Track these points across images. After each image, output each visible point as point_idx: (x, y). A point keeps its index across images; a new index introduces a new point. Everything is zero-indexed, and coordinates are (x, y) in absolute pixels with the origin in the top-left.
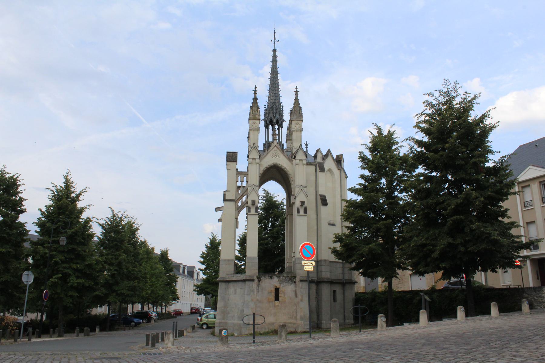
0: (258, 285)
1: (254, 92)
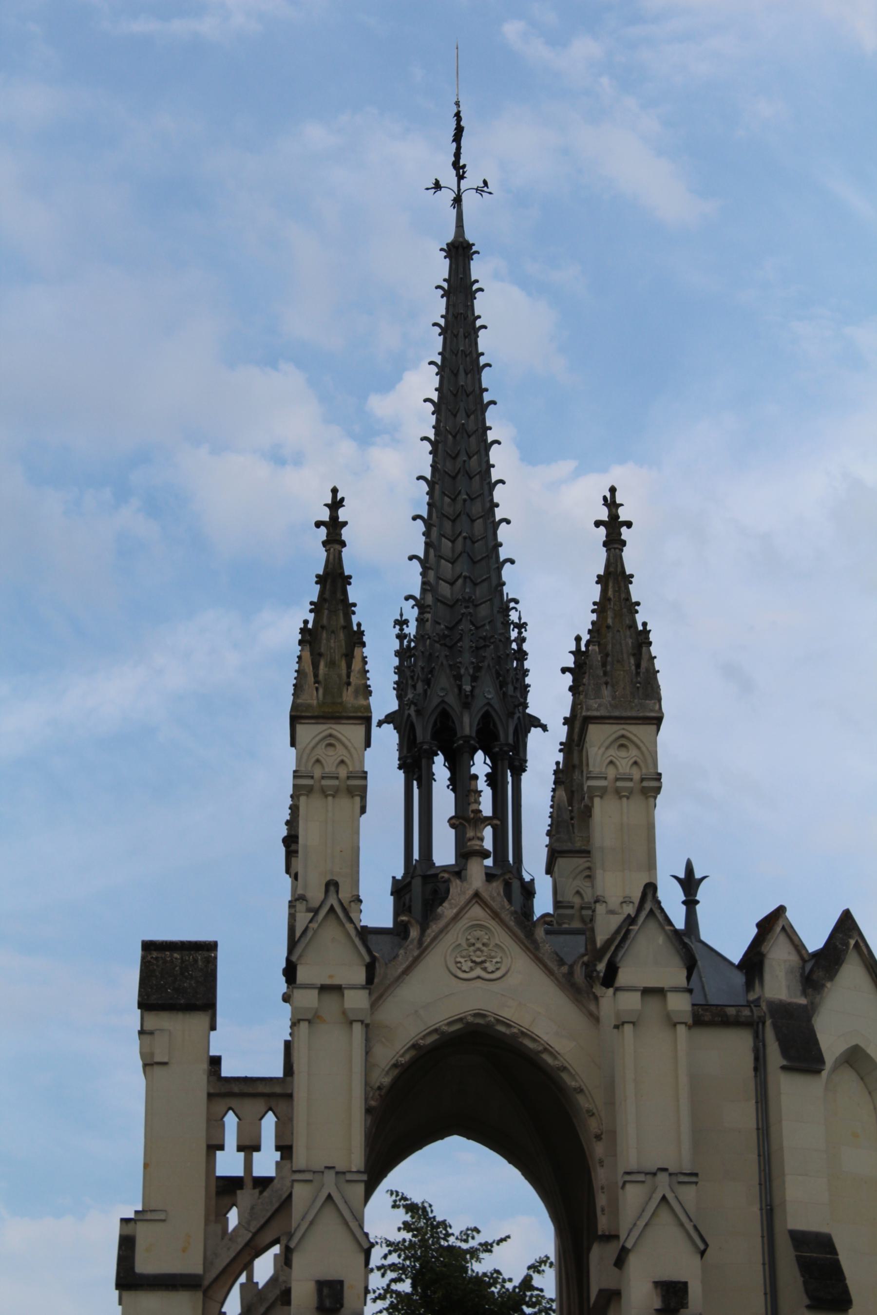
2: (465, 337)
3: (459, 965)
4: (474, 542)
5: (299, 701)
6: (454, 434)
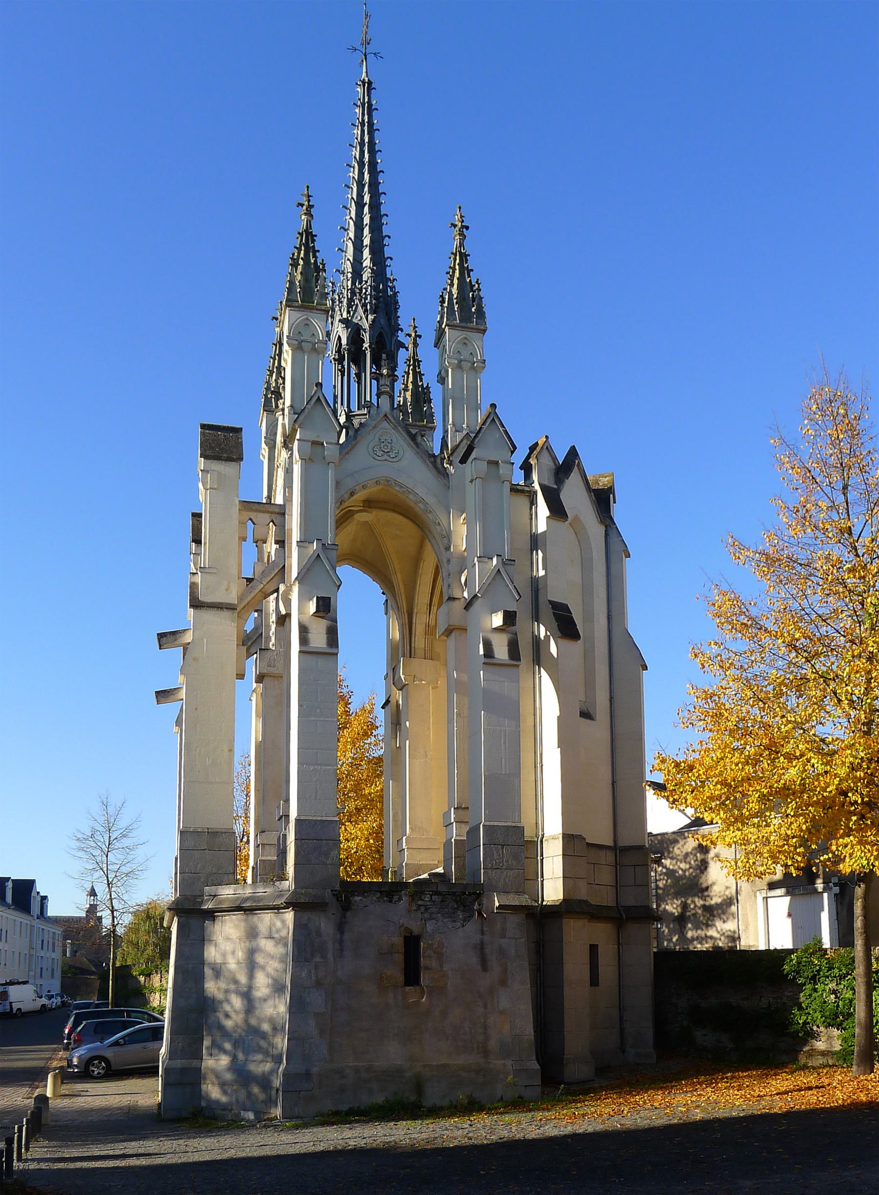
0: (341, 928)
5: (290, 297)
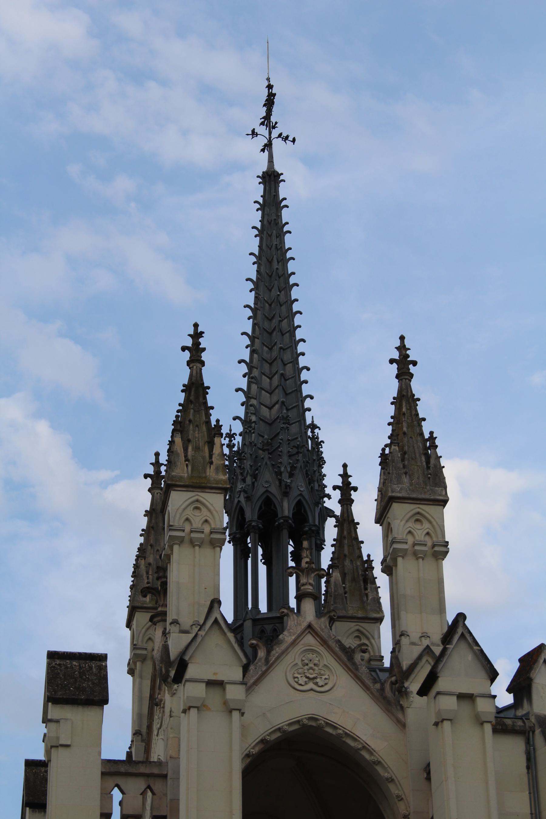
1: (187, 355)
2: (277, 237)
3: (296, 680)
4: (286, 380)
6: (270, 303)
